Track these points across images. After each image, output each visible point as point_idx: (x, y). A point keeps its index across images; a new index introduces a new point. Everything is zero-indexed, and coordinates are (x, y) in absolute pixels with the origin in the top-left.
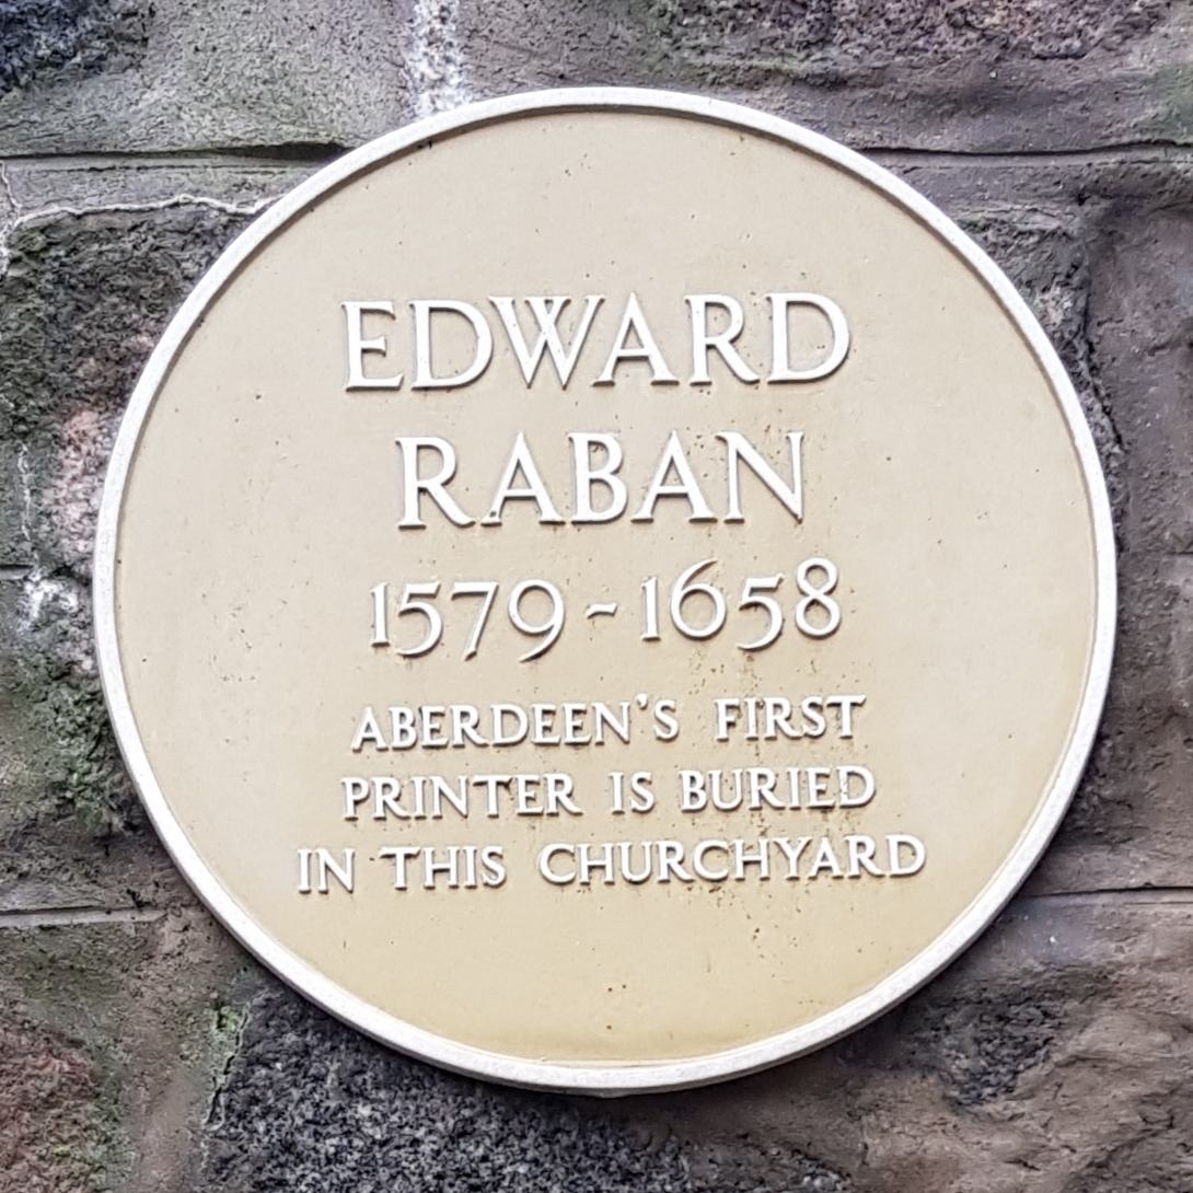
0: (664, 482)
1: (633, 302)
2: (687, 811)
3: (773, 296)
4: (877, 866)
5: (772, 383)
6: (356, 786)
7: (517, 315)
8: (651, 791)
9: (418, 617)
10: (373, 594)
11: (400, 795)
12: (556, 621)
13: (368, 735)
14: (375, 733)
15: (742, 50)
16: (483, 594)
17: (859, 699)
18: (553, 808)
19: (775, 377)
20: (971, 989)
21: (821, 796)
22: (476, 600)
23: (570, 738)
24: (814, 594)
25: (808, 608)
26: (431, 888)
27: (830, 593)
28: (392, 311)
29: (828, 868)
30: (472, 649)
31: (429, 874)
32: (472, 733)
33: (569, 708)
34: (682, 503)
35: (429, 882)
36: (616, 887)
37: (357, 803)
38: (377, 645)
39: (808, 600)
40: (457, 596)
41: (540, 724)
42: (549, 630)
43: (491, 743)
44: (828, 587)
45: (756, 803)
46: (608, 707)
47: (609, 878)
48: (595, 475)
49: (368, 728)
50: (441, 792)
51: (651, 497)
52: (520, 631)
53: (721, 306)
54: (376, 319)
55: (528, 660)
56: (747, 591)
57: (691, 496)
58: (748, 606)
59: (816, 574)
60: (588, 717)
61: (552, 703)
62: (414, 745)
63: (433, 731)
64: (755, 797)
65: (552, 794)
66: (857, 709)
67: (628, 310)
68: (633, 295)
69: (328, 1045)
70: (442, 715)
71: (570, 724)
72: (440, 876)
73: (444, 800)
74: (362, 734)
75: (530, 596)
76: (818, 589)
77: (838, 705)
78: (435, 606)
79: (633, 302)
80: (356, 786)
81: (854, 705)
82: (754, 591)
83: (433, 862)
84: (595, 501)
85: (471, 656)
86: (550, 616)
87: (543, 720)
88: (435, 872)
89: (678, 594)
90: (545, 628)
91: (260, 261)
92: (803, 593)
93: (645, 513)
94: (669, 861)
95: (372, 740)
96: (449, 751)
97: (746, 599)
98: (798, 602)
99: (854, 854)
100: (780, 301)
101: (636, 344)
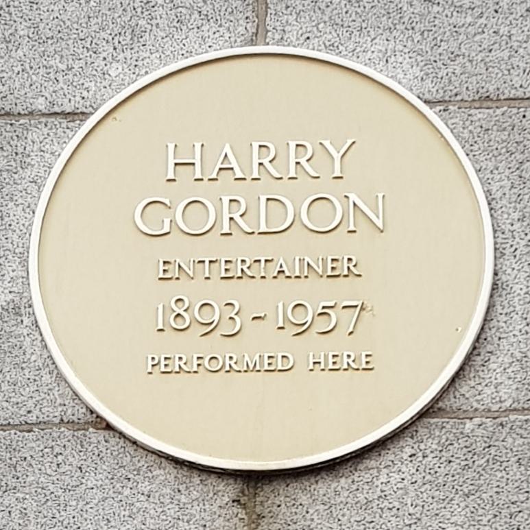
3: (222, 197)
5: (260, 233)
6: (153, 358)
7: (300, 209)
9: (325, 317)
11: (188, 308)
12: (216, 318)
15: (517, 166)
16: (356, 306)
19: (261, 231)
20: (244, 500)
22: (353, 310)
23: (364, 366)
24: (178, 311)
26: (150, 373)
27: (185, 310)
29: (283, 272)
30: (351, 330)
34: (230, 172)
37: (153, 366)
38: (280, 328)
39: (175, 314)
40: (344, 307)
42: (212, 323)
43: (361, 368)
45: (227, 368)
49: (281, 266)
51: (217, 170)
52: (199, 322)
53: (235, 200)
54: (273, 202)
56: (321, 307)
57: (235, 169)
58: (320, 314)
62: (220, 369)
65: (177, 362)
72: (317, 365)
75: (299, 308)
78: (334, 311)
80: (153, 358)
82: (324, 307)
85: (351, 333)
86: (213, 316)
90: (211, 321)
91: (77, 157)
92: (174, 311)
96: (341, 372)
97: (320, 311)
98: (171, 314)
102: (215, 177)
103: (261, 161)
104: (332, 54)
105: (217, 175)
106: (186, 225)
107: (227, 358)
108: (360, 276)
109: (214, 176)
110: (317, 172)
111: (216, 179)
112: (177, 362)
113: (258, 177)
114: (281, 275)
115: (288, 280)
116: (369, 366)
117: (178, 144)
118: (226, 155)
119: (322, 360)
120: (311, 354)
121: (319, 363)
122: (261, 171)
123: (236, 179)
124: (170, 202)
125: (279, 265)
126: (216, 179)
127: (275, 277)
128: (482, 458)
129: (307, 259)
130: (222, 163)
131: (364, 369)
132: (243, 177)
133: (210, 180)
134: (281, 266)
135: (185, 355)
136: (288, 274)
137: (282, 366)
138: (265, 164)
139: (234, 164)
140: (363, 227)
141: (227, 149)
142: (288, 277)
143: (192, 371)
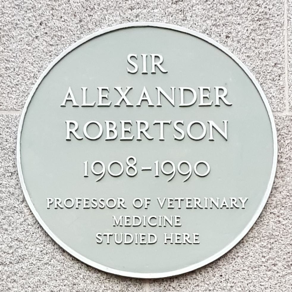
2: (187, 208)
6: (50, 200)
8: (102, 238)
10: (155, 164)
12: (104, 171)
13: (224, 205)
14: (226, 204)
17: (183, 199)
21: (178, 241)
26: (166, 244)
27: (134, 165)
28: (183, 123)
32: (122, 205)
33: (85, 199)
34: (71, 102)
41: (77, 203)
42: (102, 173)
44: (134, 164)
46: (214, 199)
47: (172, 242)
49: (224, 203)
51: (140, 100)
55: (97, 181)
59: (131, 160)
60: (82, 201)
61: (81, 197)
63: (86, 204)
64: (185, 240)
65: (185, 238)
66: (182, 201)
70: (88, 200)
71: (85, 203)
72: (169, 241)
75: (116, 165)
76: (131, 164)
77: (177, 200)
81: (181, 200)
83: (167, 237)
86: (102, 170)
87: (78, 202)
88: (167, 239)
92: (128, 165)
95: (225, 206)
99: (232, 202)
102: (140, 105)
103: (141, 130)
106: (89, 136)
107: (119, 200)
110: (132, 103)
111: (65, 106)
112: (185, 238)
113: (163, 139)
114: (224, 208)
115: (227, 209)
118: (69, 94)
119: (171, 238)
121: (170, 239)
122: (142, 135)
124: (210, 89)
125: (223, 203)
126: (65, 106)
127: (221, 208)
129: (212, 123)
130: (143, 97)
133: (83, 106)
134: (224, 203)
135: (189, 234)
136: (227, 207)
137: (150, 241)
138: (143, 132)
142: (228, 208)
143: (192, 243)
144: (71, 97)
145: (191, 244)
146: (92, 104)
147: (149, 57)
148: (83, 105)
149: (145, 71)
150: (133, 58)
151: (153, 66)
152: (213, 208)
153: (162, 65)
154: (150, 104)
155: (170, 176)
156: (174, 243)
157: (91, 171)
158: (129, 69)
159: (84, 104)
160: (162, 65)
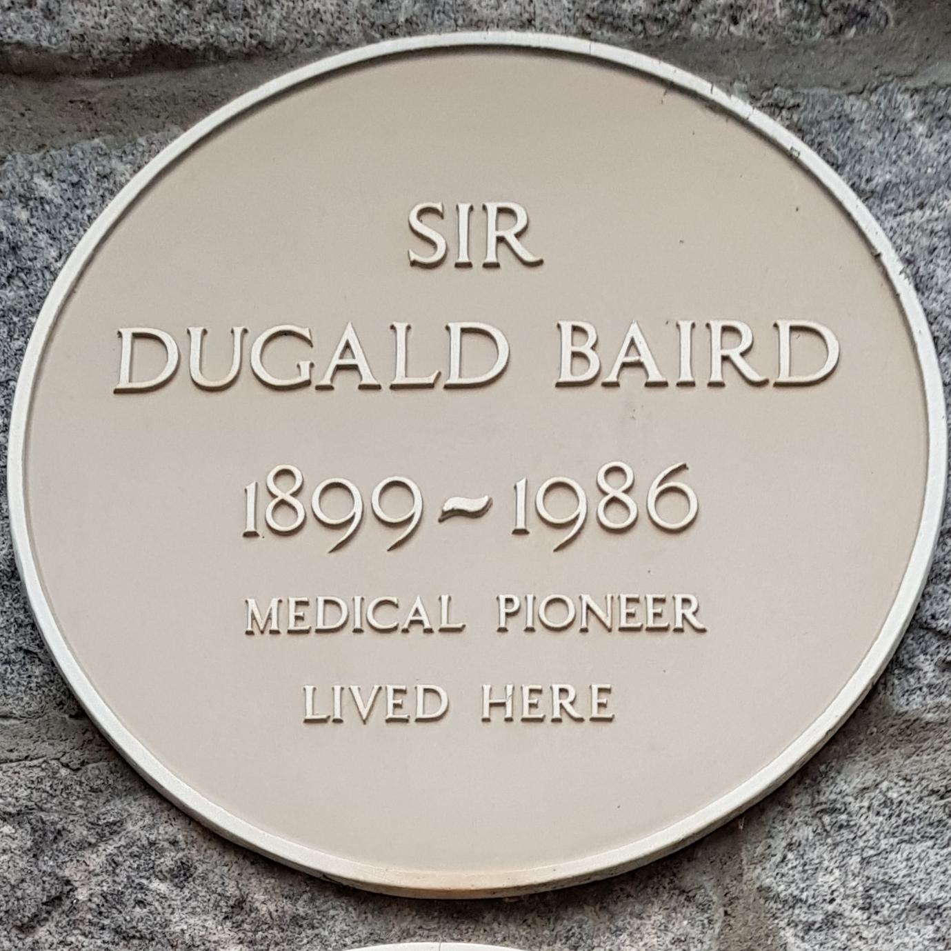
0: (627, 355)
1: (350, 328)
4: (576, 711)
6: (509, 601)
11: (525, 229)
18: (679, 624)
24: (612, 493)
25: (608, 504)
26: (486, 720)
27: (627, 491)
29: (421, 622)
31: (487, 706)
35: (486, 715)
36: (514, 723)
37: (508, 615)
39: (607, 498)
47: (509, 715)
48: (576, 349)
49: (417, 612)
50: (588, 607)
51: (408, 622)
59: (285, 479)
63: (656, 615)
67: (346, 332)
68: (350, 325)
69: (642, 886)
72: (495, 710)
73: (589, 612)
74: (411, 617)
75: (394, 491)
79: (350, 328)
80: (509, 601)
84: (574, 370)
88: (492, 705)
89: (654, 491)
93: (612, 378)
94: (561, 701)
98: (601, 500)
100: (456, 329)
101: (351, 356)
104: (509, 898)
105: (332, 379)
108: (703, 631)
109: (326, 381)
111: (330, 388)
114: (416, 630)
116: (605, 714)
117: (365, 597)
120: (487, 688)
121: (503, 705)
123: (648, 385)
126: (330, 388)
128: (907, 253)
129: (587, 598)
131: (650, 630)
132: (374, 382)
134: (417, 612)
136: (427, 625)
137: (424, 713)
139: (360, 360)
140: (593, 625)
141: (418, 604)
142: (429, 631)
144: (354, 357)
145: (581, 720)
146: (430, 380)
147: (701, 326)
148: (397, 381)
149: (463, 258)
150: (428, 218)
151: (492, 241)
152: (590, 629)
153: (749, 356)
154: (652, 379)
155: (344, 530)
156: (517, 719)
157: (263, 518)
158: (415, 253)
159: (400, 380)
160: (749, 356)
